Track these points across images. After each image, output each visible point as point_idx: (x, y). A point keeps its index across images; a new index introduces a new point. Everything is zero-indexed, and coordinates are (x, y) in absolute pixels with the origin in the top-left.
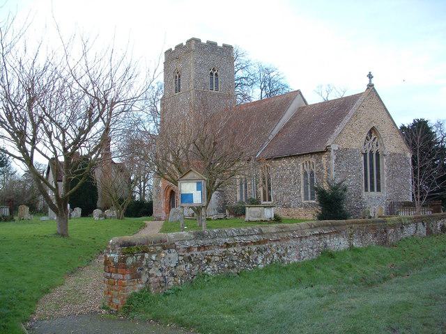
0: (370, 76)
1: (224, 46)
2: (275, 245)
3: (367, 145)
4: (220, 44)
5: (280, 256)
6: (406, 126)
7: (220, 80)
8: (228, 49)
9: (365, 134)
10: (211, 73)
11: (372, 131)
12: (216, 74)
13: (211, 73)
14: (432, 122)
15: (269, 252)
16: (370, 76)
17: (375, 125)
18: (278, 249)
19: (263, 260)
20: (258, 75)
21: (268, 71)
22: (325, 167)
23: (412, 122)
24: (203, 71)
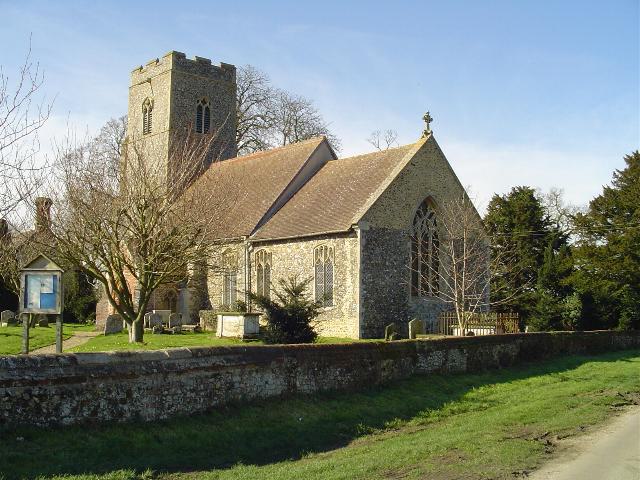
0: (428, 119)
1: (223, 65)
2: (101, 385)
3: (419, 223)
4: (216, 63)
5: (112, 402)
6: (501, 196)
7: (212, 118)
8: (228, 71)
9: (415, 209)
10: (200, 107)
11: (427, 203)
12: (207, 109)
13: (200, 108)
14: (542, 190)
15: (89, 396)
16: (428, 119)
17: (432, 193)
18: (110, 392)
19: (74, 410)
20: (279, 112)
21: (293, 107)
22: (349, 257)
23: (510, 191)
24: (186, 102)
